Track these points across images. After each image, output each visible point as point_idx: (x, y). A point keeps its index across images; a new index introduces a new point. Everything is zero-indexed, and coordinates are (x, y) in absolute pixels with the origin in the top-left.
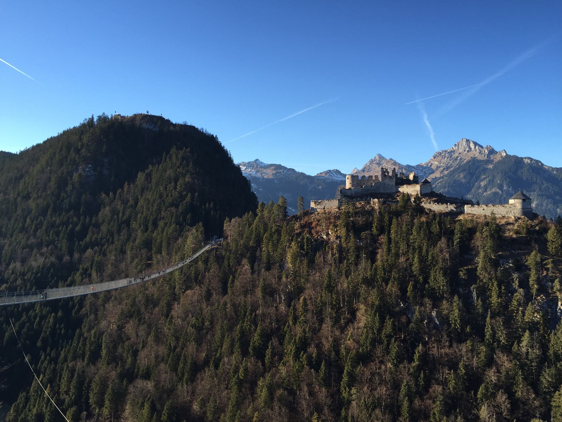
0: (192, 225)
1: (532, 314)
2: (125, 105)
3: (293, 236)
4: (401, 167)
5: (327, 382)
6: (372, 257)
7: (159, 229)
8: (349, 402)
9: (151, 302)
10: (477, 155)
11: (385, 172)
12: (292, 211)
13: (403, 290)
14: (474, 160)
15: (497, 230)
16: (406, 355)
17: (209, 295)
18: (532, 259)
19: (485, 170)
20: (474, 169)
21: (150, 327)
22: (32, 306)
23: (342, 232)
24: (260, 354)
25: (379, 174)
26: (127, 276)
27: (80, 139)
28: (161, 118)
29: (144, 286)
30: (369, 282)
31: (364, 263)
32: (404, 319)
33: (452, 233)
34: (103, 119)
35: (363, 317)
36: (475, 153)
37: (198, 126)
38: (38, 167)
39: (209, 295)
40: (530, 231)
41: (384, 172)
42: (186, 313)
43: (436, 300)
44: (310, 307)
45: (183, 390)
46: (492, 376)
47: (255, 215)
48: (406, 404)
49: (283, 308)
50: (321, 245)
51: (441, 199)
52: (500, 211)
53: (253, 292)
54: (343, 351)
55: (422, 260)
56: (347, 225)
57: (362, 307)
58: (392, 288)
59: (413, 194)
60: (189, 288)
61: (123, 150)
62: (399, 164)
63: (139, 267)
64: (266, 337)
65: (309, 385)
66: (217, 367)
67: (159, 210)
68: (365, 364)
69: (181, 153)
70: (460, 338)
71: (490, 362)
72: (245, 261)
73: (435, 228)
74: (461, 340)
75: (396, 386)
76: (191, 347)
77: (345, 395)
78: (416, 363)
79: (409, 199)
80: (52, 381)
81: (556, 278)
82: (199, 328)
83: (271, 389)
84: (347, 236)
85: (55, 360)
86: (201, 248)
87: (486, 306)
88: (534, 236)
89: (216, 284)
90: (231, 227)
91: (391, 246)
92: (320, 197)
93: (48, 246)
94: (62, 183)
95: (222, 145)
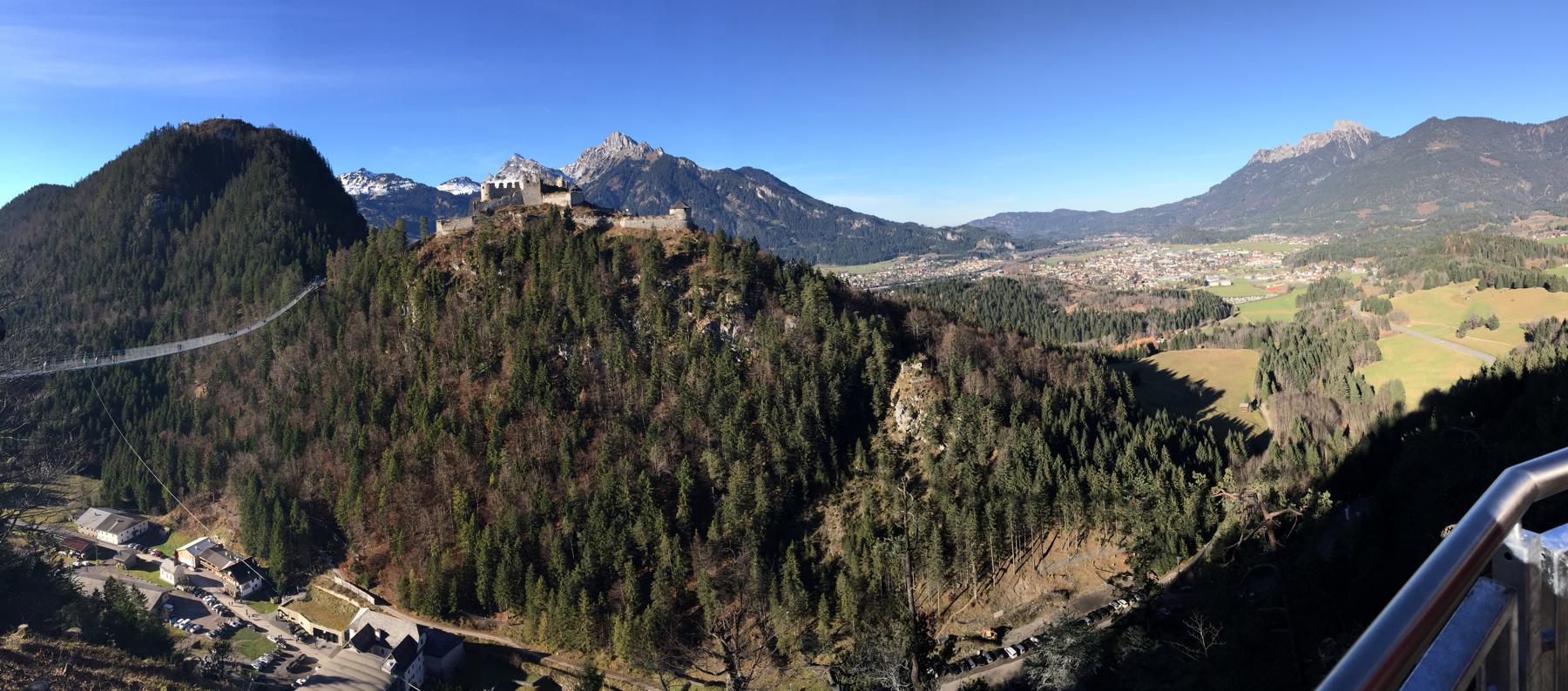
0: (286, 264)
7: (248, 270)
9: (245, 362)
14: (628, 160)
20: (626, 171)
22: (111, 369)
24: (382, 420)
26: (214, 332)
27: (143, 162)
29: (235, 344)
30: (514, 322)
35: (509, 367)
38: (98, 202)
47: (366, 244)
52: (660, 223)
55: (578, 290)
61: (195, 167)
66: (330, 435)
75: (555, 443)
86: (299, 292)
90: (336, 262)
93: (121, 298)
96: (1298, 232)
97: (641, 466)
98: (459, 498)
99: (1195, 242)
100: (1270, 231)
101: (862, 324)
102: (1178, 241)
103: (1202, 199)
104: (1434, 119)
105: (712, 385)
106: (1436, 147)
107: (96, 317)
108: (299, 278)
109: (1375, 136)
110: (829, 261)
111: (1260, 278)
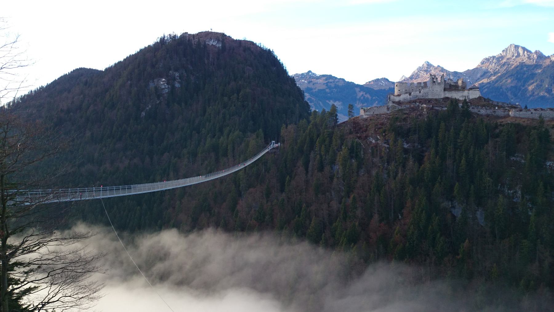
4: (449, 73)
6: (420, 160)
10: (525, 60)
11: (433, 79)
14: (522, 65)
19: (533, 75)
28: (223, 35)
36: (524, 58)
49: (335, 205)
59: (461, 99)
62: (447, 71)
63: (209, 168)
79: (457, 105)
81: (283, 142)
91: (438, 149)
95: (278, 59)
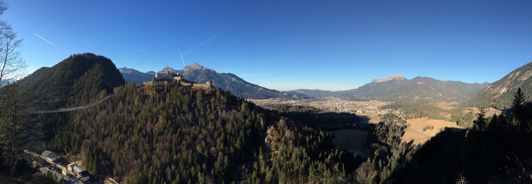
0: (103, 89)
1: (212, 117)
2: (81, 51)
3: (137, 93)
4: (175, 71)
5: (148, 142)
8: (156, 148)
9: (89, 114)
12: (137, 85)
13: (174, 111)
14: (197, 69)
15: (203, 92)
16: (175, 132)
17: (108, 113)
18: (212, 100)
20: (197, 72)
21: (89, 122)
22: (55, 113)
23: (154, 92)
24: (126, 133)
25: (167, 73)
30: (163, 109)
31: (162, 103)
32: (174, 120)
33: (190, 92)
34: (75, 55)
35: (161, 120)
36: (197, 67)
37: (104, 56)
39: (108, 113)
40: (212, 92)
41: (169, 72)
42: (101, 118)
43: (185, 113)
44: (143, 117)
45: (100, 144)
46: (200, 136)
48: (174, 148)
49: (133, 117)
50: (147, 97)
51: (187, 82)
53: (123, 112)
54: (154, 132)
55: (180, 101)
56: (156, 90)
57: (161, 117)
58: (171, 111)
60: (102, 110)
64: (128, 127)
65: (143, 143)
66: (111, 137)
67: (92, 84)
68: (161, 136)
69: (99, 65)
70: (191, 125)
71: (200, 132)
72: (121, 102)
73: (185, 91)
74: (192, 126)
75: (171, 142)
76: (103, 130)
77: (155, 146)
78: (178, 134)
80: (61, 136)
82: (105, 124)
83: (129, 145)
84: (156, 93)
85: (61, 130)
87: (199, 115)
88: (213, 94)
89: (111, 109)
90: (116, 90)
92: (147, 80)
94: (63, 76)
96: (383, 100)
97: (195, 151)
98: (145, 157)
99: (351, 100)
100: (375, 99)
101: (258, 115)
102: (349, 100)
103: (356, 90)
104: (419, 77)
105: (215, 129)
106: (419, 83)
107: (53, 100)
108: (105, 93)
109: (405, 79)
110: (251, 98)
111: (371, 111)
